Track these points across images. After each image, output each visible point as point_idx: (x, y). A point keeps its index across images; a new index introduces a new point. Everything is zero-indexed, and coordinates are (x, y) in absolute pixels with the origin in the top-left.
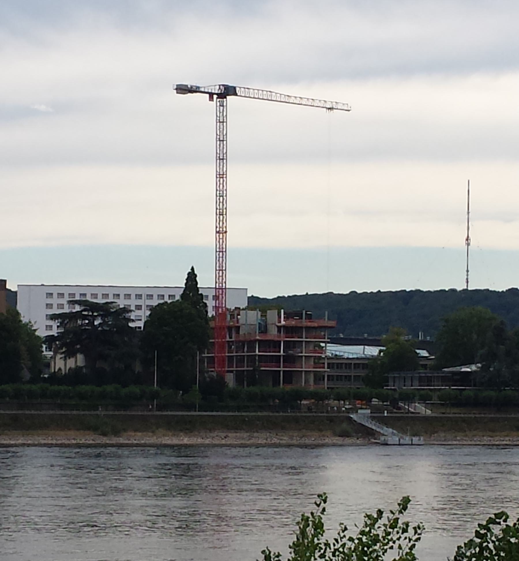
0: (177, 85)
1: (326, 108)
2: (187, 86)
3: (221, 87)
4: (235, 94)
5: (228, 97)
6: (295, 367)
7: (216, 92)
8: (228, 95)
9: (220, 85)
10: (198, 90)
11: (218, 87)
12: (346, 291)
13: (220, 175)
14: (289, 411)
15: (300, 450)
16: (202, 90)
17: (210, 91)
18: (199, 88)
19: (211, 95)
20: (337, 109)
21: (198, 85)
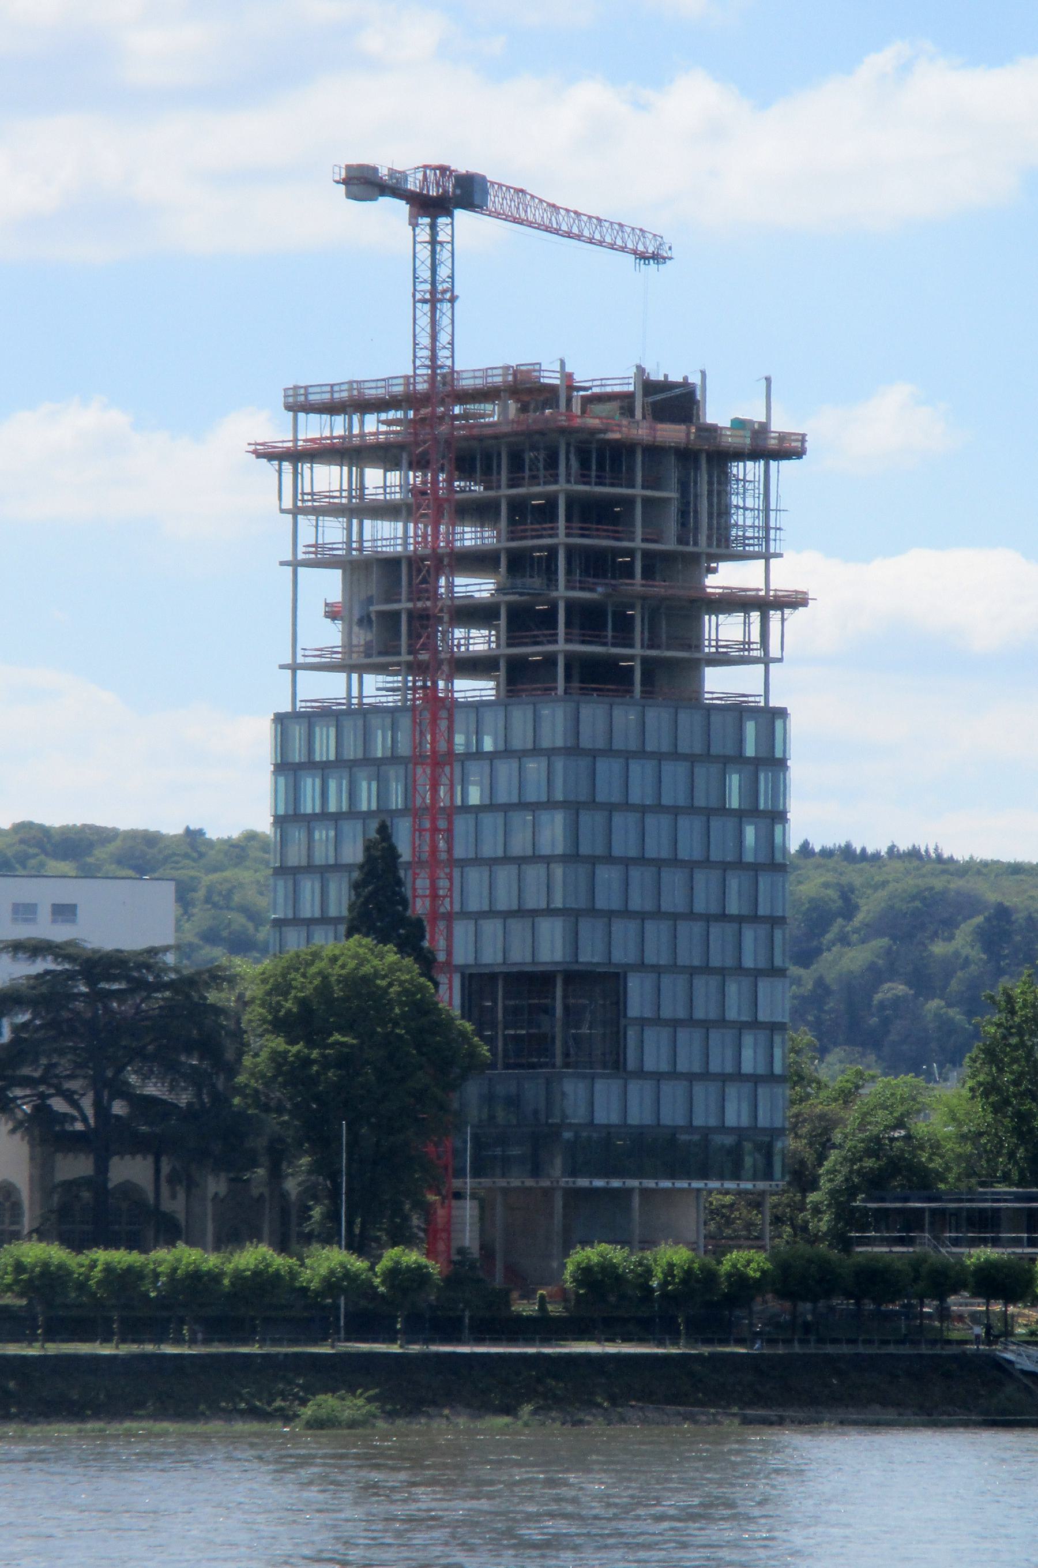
0: (349, 168)
5: (459, 213)
9: (425, 167)
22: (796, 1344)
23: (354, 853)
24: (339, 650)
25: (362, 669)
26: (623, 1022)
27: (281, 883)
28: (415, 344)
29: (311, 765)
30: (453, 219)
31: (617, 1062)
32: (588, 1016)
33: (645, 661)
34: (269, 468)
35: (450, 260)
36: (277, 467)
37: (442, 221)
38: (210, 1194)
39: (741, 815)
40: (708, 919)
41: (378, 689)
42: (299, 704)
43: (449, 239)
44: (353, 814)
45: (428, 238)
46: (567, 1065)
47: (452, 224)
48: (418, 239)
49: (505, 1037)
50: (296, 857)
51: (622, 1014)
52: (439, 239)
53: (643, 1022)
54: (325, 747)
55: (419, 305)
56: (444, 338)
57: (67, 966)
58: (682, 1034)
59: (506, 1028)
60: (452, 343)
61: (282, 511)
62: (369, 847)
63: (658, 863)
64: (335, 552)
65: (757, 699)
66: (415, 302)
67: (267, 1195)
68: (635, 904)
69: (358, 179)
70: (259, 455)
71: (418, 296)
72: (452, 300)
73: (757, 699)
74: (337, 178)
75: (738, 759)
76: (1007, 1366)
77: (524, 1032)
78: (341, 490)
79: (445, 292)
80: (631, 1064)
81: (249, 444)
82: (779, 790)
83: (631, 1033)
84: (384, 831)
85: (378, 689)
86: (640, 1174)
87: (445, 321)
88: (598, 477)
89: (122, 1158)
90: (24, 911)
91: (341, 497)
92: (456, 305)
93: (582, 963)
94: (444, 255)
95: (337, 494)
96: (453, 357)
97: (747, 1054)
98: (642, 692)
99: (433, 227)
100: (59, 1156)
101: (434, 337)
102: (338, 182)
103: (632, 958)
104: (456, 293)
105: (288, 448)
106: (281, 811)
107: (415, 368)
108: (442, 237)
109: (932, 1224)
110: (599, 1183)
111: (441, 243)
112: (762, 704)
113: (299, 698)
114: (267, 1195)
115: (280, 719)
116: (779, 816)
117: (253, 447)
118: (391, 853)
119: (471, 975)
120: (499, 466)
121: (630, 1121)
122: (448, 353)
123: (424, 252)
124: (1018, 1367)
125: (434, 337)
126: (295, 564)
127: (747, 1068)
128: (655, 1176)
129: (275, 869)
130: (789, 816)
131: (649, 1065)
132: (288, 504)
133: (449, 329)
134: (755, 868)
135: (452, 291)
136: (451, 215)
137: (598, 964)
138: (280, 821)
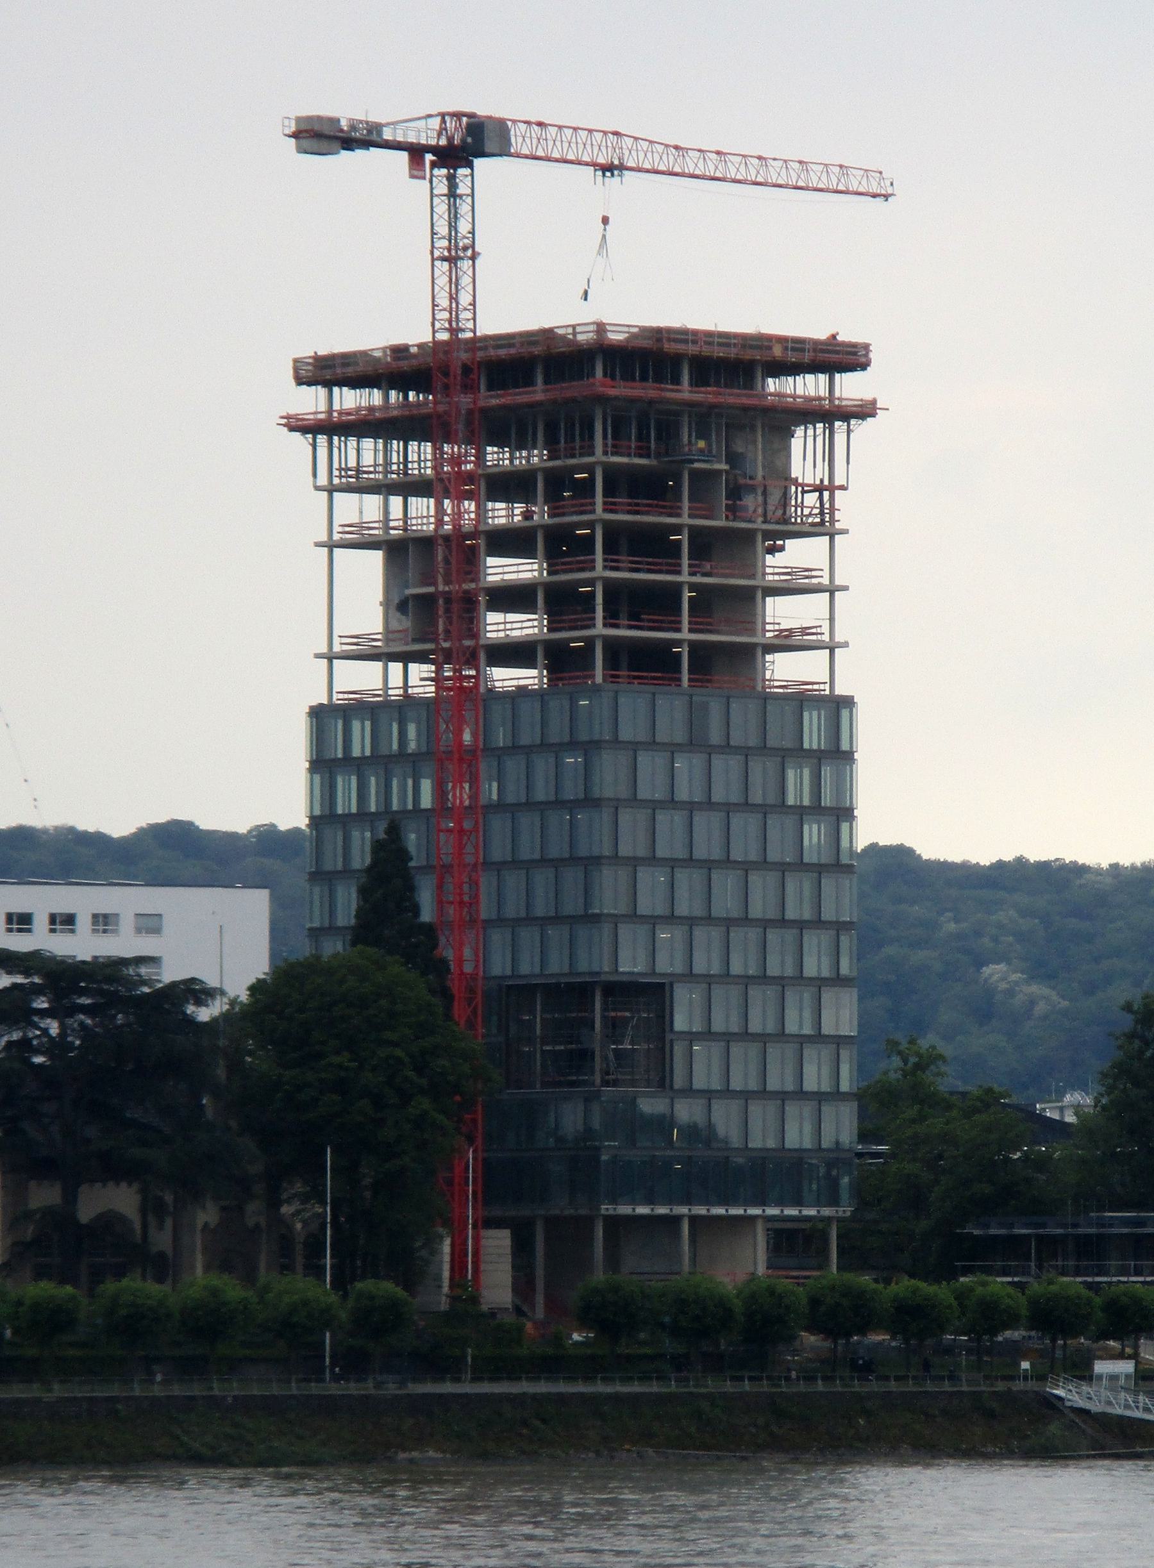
0: (299, 120)
1: (594, 165)
2: (335, 121)
3: (451, 124)
4: (504, 151)
5: (478, 162)
6: (710, 632)
7: (433, 142)
8: (483, 154)
9: (443, 115)
10: (374, 137)
11: (435, 123)
12: (133, 830)
13: (340, 469)
14: (563, 985)
15: (744, 769)
16: (387, 135)
17: (412, 139)
18: (377, 128)
19: (416, 152)
20: (639, 170)
21: (373, 118)
22: (820, 1382)
23: (361, 858)
24: (379, 637)
25: (406, 658)
26: (669, 1036)
27: (317, 890)
28: (434, 305)
29: (348, 762)
30: (472, 170)
31: (663, 1079)
32: (630, 1032)
33: (694, 647)
34: (301, 442)
35: (470, 214)
36: (311, 441)
37: (462, 171)
38: (200, 1224)
39: (801, 813)
40: (765, 924)
41: (422, 679)
42: (335, 696)
43: (469, 191)
44: (362, 816)
45: (445, 191)
46: (606, 1083)
47: (472, 175)
48: (435, 192)
49: (543, 1052)
50: (333, 862)
51: (667, 1029)
52: (459, 192)
53: (691, 1037)
54: (361, 744)
55: (438, 263)
56: (465, 299)
57: (19, 979)
58: (736, 1049)
59: (543, 1043)
60: (474, 304)
61: (317, 488)
62: (378, 847)
63: (709, 865)
64: (371, 532)
65: (822, 687)
66: (433, 260)
67: (263, 1223)
68: (682, 910)
69: (306, 131)
70: (292, 429)
71: (437, 254)
72: (473, 258)
73: (822, 687)
74: (287, 132)
75: (798, 752)
76: (1056, 1402)
77: (562, 1048)
78: (375, 465)
79: (465, 249)
80: (679, 1082)
81: (282, 417)
82: (844, 785)
83: (679, 1049)
84: (394, 831)
85: (422, 679)
86: (688, 1201)
87: (466, 281)
88: (614, 446)
89: (104, 1186)
90: (21, 921)
91: (375, 472)
92: (477, 262)
93: (623, 973)
94: (464, 208)
95: (372, 469)
96: (474, 319)
97: (810, 1070)
98: (690, 680)
99: (452, 180)
100: (33, 1184)
101: (454, 298)
102: (290, 136)
103: (679, 968)
104: (477, 249)
105: (321, 420)
106: (317, 812)
107: (434, 332)
108: (463, 189)
109: (1038, 1251)
110: (719, 1211)
111: (461, 196)
112: (827, 692)
113: (335, 690)
114: (263, 1223)
115: (318, 714)
116: (844, 813)
117: (284, 421)
118: (403, 855)
119: (509, 987)
120: (535, 434)
121: (788, 1145)
122: (469, 315)
123: (442, 208)
124: (1068, 1404)
125: (454, 298)
126: (331, 546)
127: (810, 1085)
128: (708, 1203)
129: (311, 874)
130: (856, 813)
131: (699, 1083)
132: (323, 480)
133: (470, 288)
134: (819, 869)
135: (473, 246)
136: (470, 165)
137: (639, 974)
138: (315, 821)
